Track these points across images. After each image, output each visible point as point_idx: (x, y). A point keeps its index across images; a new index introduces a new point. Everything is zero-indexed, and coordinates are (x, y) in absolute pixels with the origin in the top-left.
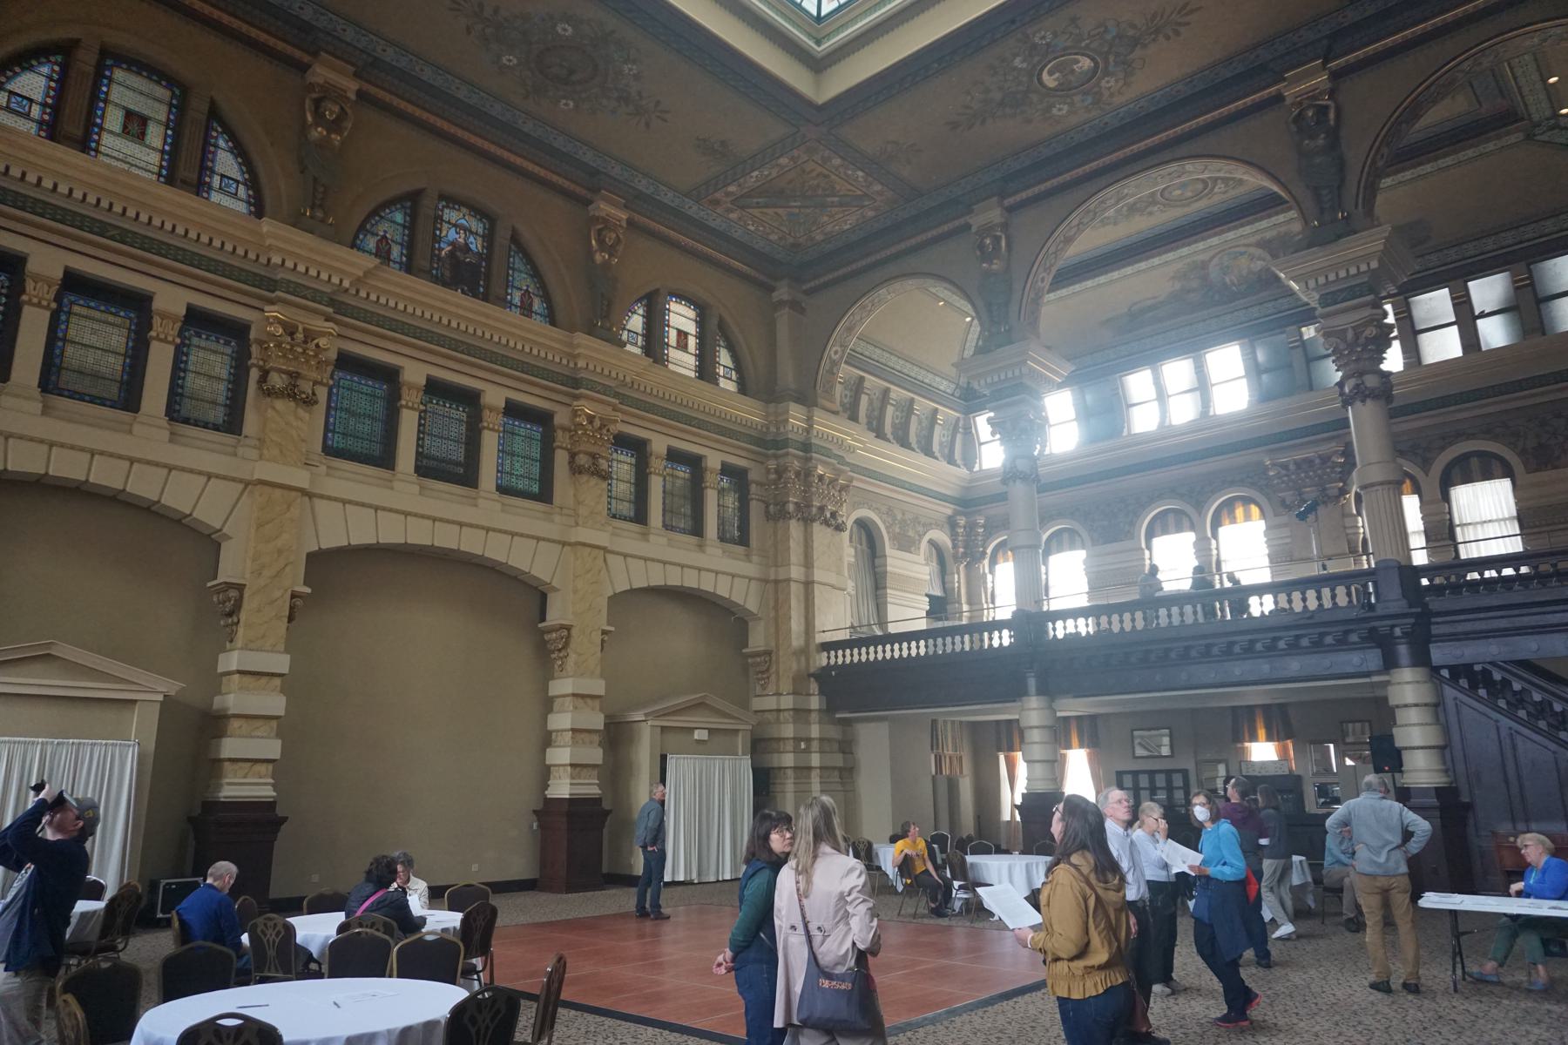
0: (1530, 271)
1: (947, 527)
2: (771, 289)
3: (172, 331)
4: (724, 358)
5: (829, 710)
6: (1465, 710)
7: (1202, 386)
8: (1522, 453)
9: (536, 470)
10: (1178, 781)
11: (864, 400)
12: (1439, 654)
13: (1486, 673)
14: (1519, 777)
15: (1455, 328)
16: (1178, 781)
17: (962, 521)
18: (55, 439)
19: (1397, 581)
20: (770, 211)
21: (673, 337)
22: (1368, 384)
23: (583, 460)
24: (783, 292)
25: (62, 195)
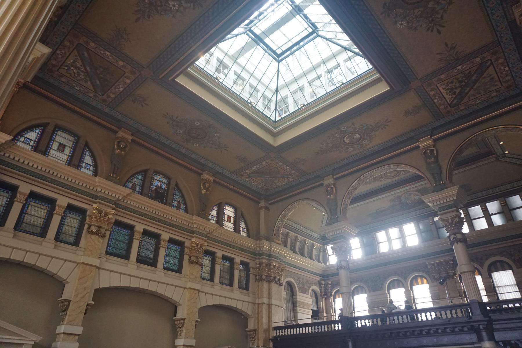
1: (318, 285)
2: (259, 203)
3: (61, 211)
4: (243, 225)
7: (402, 237)
8: (514, 261)
20: (259, 178)
24: (262, 204)
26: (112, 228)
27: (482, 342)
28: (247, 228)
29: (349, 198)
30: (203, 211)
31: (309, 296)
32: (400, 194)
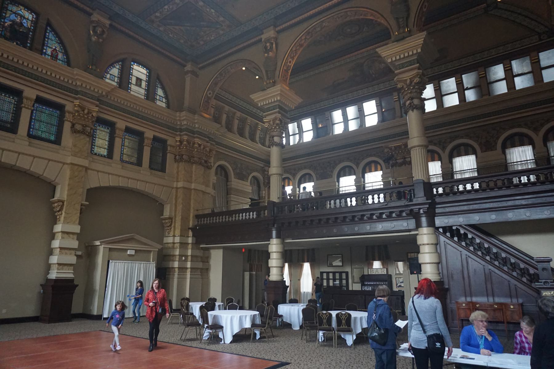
0: (485, 71)
2: (185, 66)
3: (30, 103)
4: (160, 92)
5: (196, 243)
6: (449, 247)
7: (361, 116)
8: (480, 144)
9: (54, 129)
10: (344, 276)
12: (439, 221)
13: (458, 230)
14: (469, 277)
15: (457, 94)
16: (344, 276)
18: (20, 151)
19: (422, 189)
20: (177, 27)
21: (134, 80)
23: (78, 127)
24: (189, 67)
25: (35, 70)
26: (33, 106)
27: (419, 229)
28: (167, 97)
29: (293, 58)
30: (92, 65)
31: (248, 183)
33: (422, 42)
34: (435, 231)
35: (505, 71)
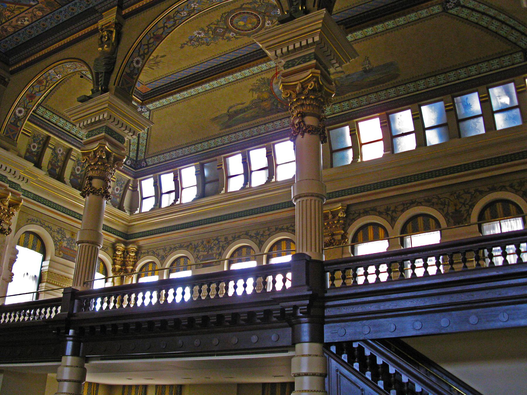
1: (110, 250)
8: (446, 216)
11: (48, 153)
13: (361, 349)
15: (414, 135)
17: (121, 247)
22: (307, 123)
32: (269, 76)
33: (320, 25)
34: (324, 352)
35: (481, 102)
